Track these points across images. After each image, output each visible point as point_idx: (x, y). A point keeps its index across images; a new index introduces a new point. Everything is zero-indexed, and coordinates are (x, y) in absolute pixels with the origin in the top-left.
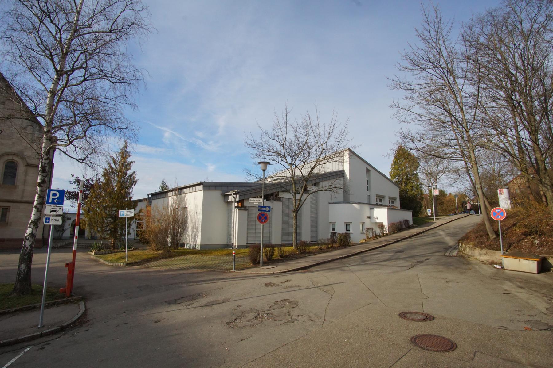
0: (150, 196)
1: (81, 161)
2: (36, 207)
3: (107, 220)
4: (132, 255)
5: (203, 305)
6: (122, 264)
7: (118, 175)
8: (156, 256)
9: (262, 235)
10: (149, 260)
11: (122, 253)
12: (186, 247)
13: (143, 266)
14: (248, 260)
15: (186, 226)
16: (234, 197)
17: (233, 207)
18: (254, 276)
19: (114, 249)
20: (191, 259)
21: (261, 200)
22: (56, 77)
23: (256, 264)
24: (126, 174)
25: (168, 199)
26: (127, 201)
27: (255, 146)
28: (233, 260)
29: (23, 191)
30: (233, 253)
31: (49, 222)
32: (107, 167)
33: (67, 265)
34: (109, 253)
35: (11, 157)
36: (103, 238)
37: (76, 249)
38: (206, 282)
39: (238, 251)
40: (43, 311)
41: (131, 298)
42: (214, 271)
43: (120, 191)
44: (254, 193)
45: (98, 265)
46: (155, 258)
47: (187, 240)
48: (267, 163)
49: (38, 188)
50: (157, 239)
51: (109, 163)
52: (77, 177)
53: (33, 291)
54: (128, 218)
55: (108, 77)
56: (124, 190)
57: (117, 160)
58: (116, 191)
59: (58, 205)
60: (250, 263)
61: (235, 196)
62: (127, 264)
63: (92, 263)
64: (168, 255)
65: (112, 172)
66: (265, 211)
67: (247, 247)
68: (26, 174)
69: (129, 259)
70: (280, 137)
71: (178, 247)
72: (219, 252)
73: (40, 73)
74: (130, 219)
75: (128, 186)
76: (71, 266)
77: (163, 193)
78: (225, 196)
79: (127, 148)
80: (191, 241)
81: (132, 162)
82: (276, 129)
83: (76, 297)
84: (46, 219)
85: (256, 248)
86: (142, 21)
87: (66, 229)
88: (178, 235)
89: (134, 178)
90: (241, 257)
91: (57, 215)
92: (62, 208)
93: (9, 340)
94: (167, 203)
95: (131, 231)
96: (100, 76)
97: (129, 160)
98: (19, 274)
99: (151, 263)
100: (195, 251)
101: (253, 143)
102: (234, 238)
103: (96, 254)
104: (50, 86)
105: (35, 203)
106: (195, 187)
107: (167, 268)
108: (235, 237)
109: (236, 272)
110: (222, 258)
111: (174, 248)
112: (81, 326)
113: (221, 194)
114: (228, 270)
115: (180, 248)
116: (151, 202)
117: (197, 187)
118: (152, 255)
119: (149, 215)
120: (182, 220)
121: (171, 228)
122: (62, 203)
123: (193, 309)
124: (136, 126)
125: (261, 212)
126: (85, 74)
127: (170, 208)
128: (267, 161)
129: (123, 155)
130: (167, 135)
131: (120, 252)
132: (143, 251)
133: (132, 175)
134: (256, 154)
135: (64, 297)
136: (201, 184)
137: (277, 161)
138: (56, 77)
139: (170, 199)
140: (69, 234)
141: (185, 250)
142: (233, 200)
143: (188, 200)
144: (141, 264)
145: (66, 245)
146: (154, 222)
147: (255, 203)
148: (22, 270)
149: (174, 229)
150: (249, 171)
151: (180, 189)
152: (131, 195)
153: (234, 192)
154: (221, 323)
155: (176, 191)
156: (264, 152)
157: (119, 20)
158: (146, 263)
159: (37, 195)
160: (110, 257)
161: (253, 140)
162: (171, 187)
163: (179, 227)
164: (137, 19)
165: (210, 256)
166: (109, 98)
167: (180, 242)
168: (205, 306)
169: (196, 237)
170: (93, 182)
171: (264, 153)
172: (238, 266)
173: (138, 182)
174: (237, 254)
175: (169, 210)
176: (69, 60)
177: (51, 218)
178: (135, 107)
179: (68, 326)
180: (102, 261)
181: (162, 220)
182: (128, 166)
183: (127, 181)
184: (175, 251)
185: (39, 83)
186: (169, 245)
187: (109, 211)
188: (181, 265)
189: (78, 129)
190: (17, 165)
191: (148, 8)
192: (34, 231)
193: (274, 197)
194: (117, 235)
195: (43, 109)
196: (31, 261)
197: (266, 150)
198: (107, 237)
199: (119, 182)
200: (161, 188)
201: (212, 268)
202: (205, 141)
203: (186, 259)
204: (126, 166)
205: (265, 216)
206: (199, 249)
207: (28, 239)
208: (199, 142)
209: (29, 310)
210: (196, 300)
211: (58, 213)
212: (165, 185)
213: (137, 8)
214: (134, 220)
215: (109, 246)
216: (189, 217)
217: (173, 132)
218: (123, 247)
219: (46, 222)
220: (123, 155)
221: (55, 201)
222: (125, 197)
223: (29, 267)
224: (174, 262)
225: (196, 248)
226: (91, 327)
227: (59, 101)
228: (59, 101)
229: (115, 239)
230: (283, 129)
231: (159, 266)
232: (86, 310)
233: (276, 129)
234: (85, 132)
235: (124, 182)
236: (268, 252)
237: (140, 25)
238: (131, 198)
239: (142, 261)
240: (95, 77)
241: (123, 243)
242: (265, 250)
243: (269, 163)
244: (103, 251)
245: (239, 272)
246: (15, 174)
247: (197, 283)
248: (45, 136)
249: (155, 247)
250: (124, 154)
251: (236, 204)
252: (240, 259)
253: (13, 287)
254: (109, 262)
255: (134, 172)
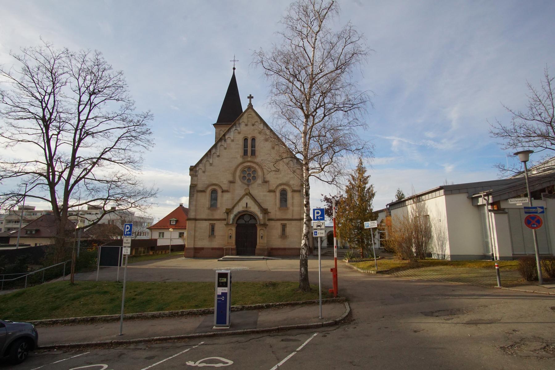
0: (388, 206)
1: (330, 183)
2: (305, 223)
3: (354, 231)
4: (381, 264)
5: (465, 322)
6: (373, 272)
7: (358, 190)
8: (404, 265)
9: (535, 244)
10: (398, 269)
11: (371, 262)
12: (433, 257)
13: (392, 275)
14: (518, 275)
15: (431, 235)
16: (485, 199)
17: (486, 211)
18: (532, 296)
19: (363, 257)
20: (441, 270)
21: (527, 200)
22: (305, 120)
23: (532, 281)
24: (365, 187)
25: (407, 208)
26: (369, 212)
27: (506, 133)
28: (497, 274)
29: (293, 210)
30: (495, 266)
31: (317, 235)
32: (348, 184)
33: (332, 270)
34: (359, 262)
35: (283, 187)
36: (353, 248)
37: (336, 257)
38: (464, 297)
39: (502, 263)
40: (321, 306)
41: (386, 305)
42: (473, 285)
43: (362, 205)
44: (513, 191)
45: (353, 271)
46: (403, 267)
47: (433, 250)
48: (527, 153)
49: (305, 208)
50: (402, 248)
51: (349, 181)
52: (326, 196)
53: (311, 289)
54: (372, 228)
55: (340, 108)
56: (365, 203)
57: (356, 176)
58: (359, 204)
59: (321, 221)
60: (521, 279)
61: (486, 198)
62: (378, 272)
63: (348, 270)
64: (415, 265)
65: (353, 188)
66: (537, 213)
67: (514, 258)
68: (293, 198)
69: (379, 268)
70: (543, 115)
71: (424, 257)
72: (475, 264)
73: (295, 120)
74: (374, 229)
75: (368, 199)
76: (334, 271)
77: (400, 202)
78: (473, 198)
79: (362, 164)
80: (438, 252)
81: (368, 177)
82: (535, 106)
83: (341, 298)
84: (315, 232)
85: (529, 261)
86: (360, 49)
87: (323, 240)
88: (424, 245)
89: (372, 191)
90: (507, 271)
91: (321, 229)
92: (324, 223)
93: (303, 325)
94: (406, 212)
95: (376, 241)
96: (335, 109)
97: (366, 175)
98: (301, 275)
99: (399, 272)
100: (445, 262)
101: (502, 131)
102: (493, 247)
103: (349, 262)
104: (302, 128)
105: (305, 220)
106: (434, 193)
107: (417, 279)
108: (495, 247)
109: (503, 288)
110: (480, 271)
111: (421, 258)
112: (350, 323)
113: (467, 197)
114: (492, 285)
115: (427, 258)
116: (390, 212)
117: (437, 192)
118: (399, 264)
119: (389, 226)
120: (425, 229)
121: (414, 237)
122: (323, 219)
123: (453, 325)
124: (371, 145)
125: (528, 215)
126: (324, 111)
127: (411, 217)
128: (526, 149)
129: (360, 171)
130: (395, 143)
131: (368, 260)
132: (390, 260)
133: (369, 188)
134: (509, 143)
135: (332, 297)
136: (441, 188)
137: (544, 146)
138: (305, 120)
139: (409, 207)
140: (326, 244)
141: (433, 260)
142: (485, 202)
143: (429, 207)
144: (390, 273)
145: (325, 253)
146: (397, 231)
147: (517, 205)
148: (303, 272)
149: (417, 238)
150: (502, 166)
151: (419, 196)
152: (372, 207)
153: (485, 194)
154: (493, 346)
155: (414, 199)
156: (520, 139)
157: (342, 57)
158: (394, 272)
159: (305, 214)
160: (362, 264)
161: (501, 128)
162: (407, 196)
163: (423, 236)
164: (356, 49)
165: (464, 268)
166: (344, 125)
167: (427, 252)
168: (468, 323)
169: (444, 246)
170: (338, 198)
171: (520, 140)
172: (505, 282)
173: (376, 194)
174: (501, 267)
175: (410, 219)
176: (312, 105)
177: (318, 231)
178: (366, 127)
179: (340, 321)
180: (355, 268)
181: (404, 230)
182: (365, 181)
183: (366, 195)
184: (423, 261)
185: (295, 128)
186: (415, 255)
187: (355, 223)
188: (431, 276)
189: (326, 159)
190: (286, 192)
191: (364, 35)
192: (306, 242)
193: (547, 193)
194: (365, 245)
195: (301, 148)
196: (307, 265)
197: (523, 135)
198: (356, 246)
199: (359, 196)
200: (397, 197)
201: (469, 282)
202: (437, 140)
203: (436, 271)
204: (363, 181)
205: (536, 220)
206: (449, 259)
207: (303, 248)
208: (430, 143)
209: (311, 304)
210: (456, 316)
211: (322, 227)
212: (400, 193)
213: (353, 39)
214: (377, 230)
215: (358, 255)
216: (433, 225)
217: (401, 139)
218: (370, 256)
219: (315, 235)
220: (360, 171)
221: (319, 218)
222: (366, 209)
223: (306, 269)
224: (423, 273)
225: (446, 258)
226: (357, 326)
227: (310, 138)
228: (310, 138)
229: (363, 248)
230: (546, 103)
231: (408, 276)
232: (351, 310)
233: (535, 106)
234: (332, 159)
235: (364, 195)
236: (550, 267)
237: (359, 53)
238: (371, 210)
239: (391, 269)
240: (332, 111)
241: (370, 252)
242: (543, 262)
243: (532, 152)
244: (354, 259)
245: (507, 289)
246: (286, 199)
247: (454, 297)
248: (304, 168)
249: (401, 256)
250: (361, 170)
251: (490, 207)
252: (506, 273)
253: (299, 285)
254: (362, 270)
255: (372, 186)
